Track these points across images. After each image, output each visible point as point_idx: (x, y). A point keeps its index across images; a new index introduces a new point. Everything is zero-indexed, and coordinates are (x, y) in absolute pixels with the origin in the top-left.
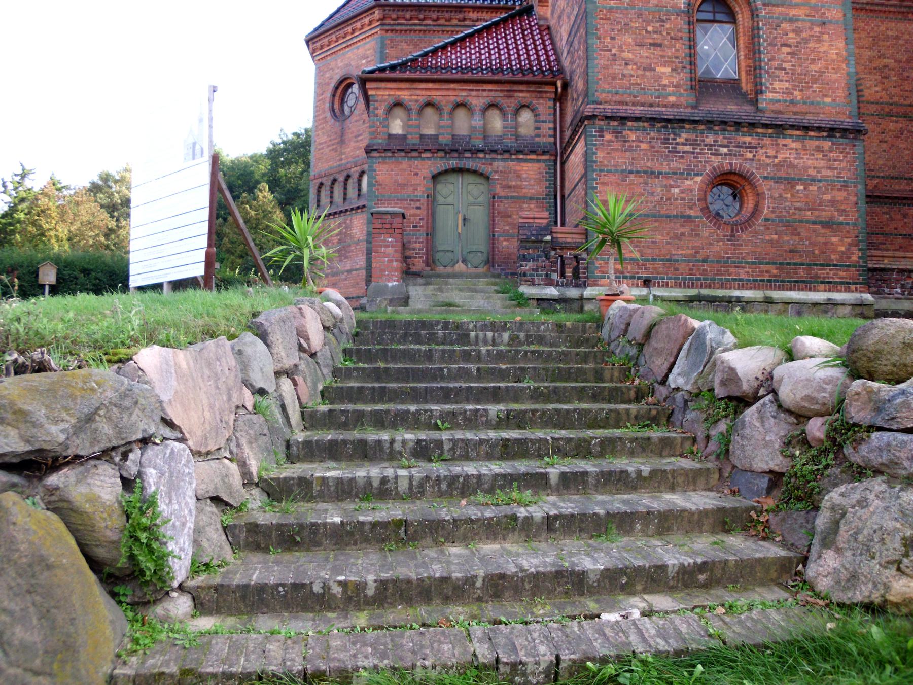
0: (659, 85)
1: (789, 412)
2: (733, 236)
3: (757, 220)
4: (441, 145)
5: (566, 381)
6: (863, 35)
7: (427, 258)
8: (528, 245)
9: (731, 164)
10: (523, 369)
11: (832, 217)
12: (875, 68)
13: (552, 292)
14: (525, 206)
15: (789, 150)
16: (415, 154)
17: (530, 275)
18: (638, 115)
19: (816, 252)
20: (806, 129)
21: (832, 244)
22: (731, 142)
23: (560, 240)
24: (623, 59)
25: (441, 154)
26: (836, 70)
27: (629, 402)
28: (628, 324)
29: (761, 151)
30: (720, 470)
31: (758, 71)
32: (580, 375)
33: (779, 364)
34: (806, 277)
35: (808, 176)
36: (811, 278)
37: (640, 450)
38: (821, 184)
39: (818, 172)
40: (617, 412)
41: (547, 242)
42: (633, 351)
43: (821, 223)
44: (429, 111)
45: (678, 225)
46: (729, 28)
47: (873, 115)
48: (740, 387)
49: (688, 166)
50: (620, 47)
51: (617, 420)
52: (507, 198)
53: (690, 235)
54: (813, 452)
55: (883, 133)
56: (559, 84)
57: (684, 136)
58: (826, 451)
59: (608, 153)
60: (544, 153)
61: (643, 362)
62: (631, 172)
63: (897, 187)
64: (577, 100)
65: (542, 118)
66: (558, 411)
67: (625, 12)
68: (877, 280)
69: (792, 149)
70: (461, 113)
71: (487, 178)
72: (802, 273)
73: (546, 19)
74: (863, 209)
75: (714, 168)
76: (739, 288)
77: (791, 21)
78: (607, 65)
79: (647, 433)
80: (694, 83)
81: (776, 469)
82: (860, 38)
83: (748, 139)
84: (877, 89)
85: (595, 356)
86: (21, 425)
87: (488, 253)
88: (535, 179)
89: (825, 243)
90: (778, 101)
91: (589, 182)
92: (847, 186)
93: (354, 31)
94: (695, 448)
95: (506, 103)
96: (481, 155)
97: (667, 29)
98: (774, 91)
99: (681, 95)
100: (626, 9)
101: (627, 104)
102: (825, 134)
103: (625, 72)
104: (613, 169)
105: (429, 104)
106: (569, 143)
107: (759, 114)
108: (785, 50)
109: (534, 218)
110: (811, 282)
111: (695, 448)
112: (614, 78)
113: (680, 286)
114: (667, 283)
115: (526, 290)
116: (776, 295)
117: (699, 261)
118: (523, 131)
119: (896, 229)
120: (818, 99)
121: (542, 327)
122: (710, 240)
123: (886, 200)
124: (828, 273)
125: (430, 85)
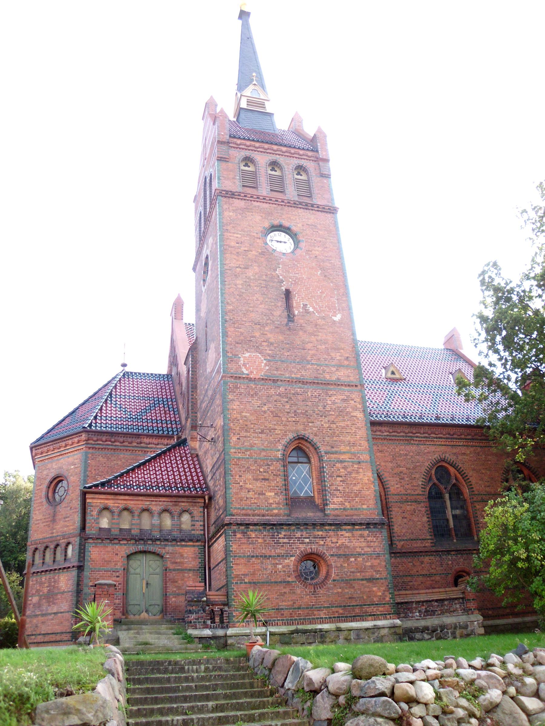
0: (268, 503)
1: (333, 695)
2: (315, 591)
3: (329, 581)
4: (133, 536)
5: (237, 689)
6: (387, 454)
7: (123, 610)
8: (192, 603)
9: (311, 549)
10: (216, 685)
11: (372, 575)
12: (395, 474)
13: (207, 632)
14: (186, 575)
15: (344, 538)
16: (116, 541)
17: (194, 622)
18: (256, 522)
19: (365, 597)
20: (354, 524)
21: (374, 591)
22: (311, 536)
23: (212, 600)
24: (247, 488)
25: (133, 541)
26: (368, 489)
27: (268, 697)
28: (263, 659)
29: (328, 540)
30: (309, 722)
31: (324, 492)
32: (243, 685)
33: (329, 675)
34: (360, 613)
35: (357, 552)
36: (363, 613)
37: (275, 717)
38: (364, 557)
39: (362, 549)
40: (264, 702)
41: (204, 601)
42: (267, 672)
43: (366, 579)
44: (125, 513)
45: (282, 588)
46: (307, 466)
47: (397, 502)
48: (314, 686)
49: (286, 551)
50: (245, 481)
51: (263, 705)
52: (174, 570)
53: (290, 593)
54: (342, 709)
55: (404, 512)
56: (207, 497)
57: (283, 533)
58: (345, 708)
59: (239, 546)
60: (197, 541)
61: (272, 677)
62: (253, 556)
63: (415, 545)
64: (219, 510)
65: (196, 519)
66: (238, 703)
67: (247, 460)
68: (404, 609)
69: (346, 537)
70: (145, 515)
71: (162, 557)
72: (357, 611)
73: (195, 449)
74: (390, 569)
75: (301, 551)
76: (320, 623)
77: (341, 462)
78: (237, 492)
79: (277, 710)
80: (288, 501)
81: (329, 718)
82: (385, 456)
83: (320, 533)
84: (397, 486)
85: (248, 676)
86: (78, 714)
87: (162, 606)
88: (192, 558)
89: (369, 592)
90: (337, 509)
91: (228, 563)
92: (379, 556)
93: (66, 446)
94: (298, 715)
95: (174, 509)
96: (158, 543)
97: (271, 470)
98: (334, 503)
99: (281, 509)
100: (248, 458)
101: (249, 515)
102: (364, 527)
103: (248, 496)
104: (242, 555)
105: (126, 509)
106: (213, 536)
107: (326, 517)
108: (339, 479)
109: (195, 587)
110: (363, 616)
111: (298, 715)
112: (241, 500)
113: (285, 625)
114: (277, 623)
115: (190, 631)
116: (343, 625)
117: (296, 608)
118: (184, 527)
119: (417, 571)
120: (359, 507)
121: (219, 661)
122: (301, 594)
123: (410, 554)
124: (372, 610)
125: (127, 497)
